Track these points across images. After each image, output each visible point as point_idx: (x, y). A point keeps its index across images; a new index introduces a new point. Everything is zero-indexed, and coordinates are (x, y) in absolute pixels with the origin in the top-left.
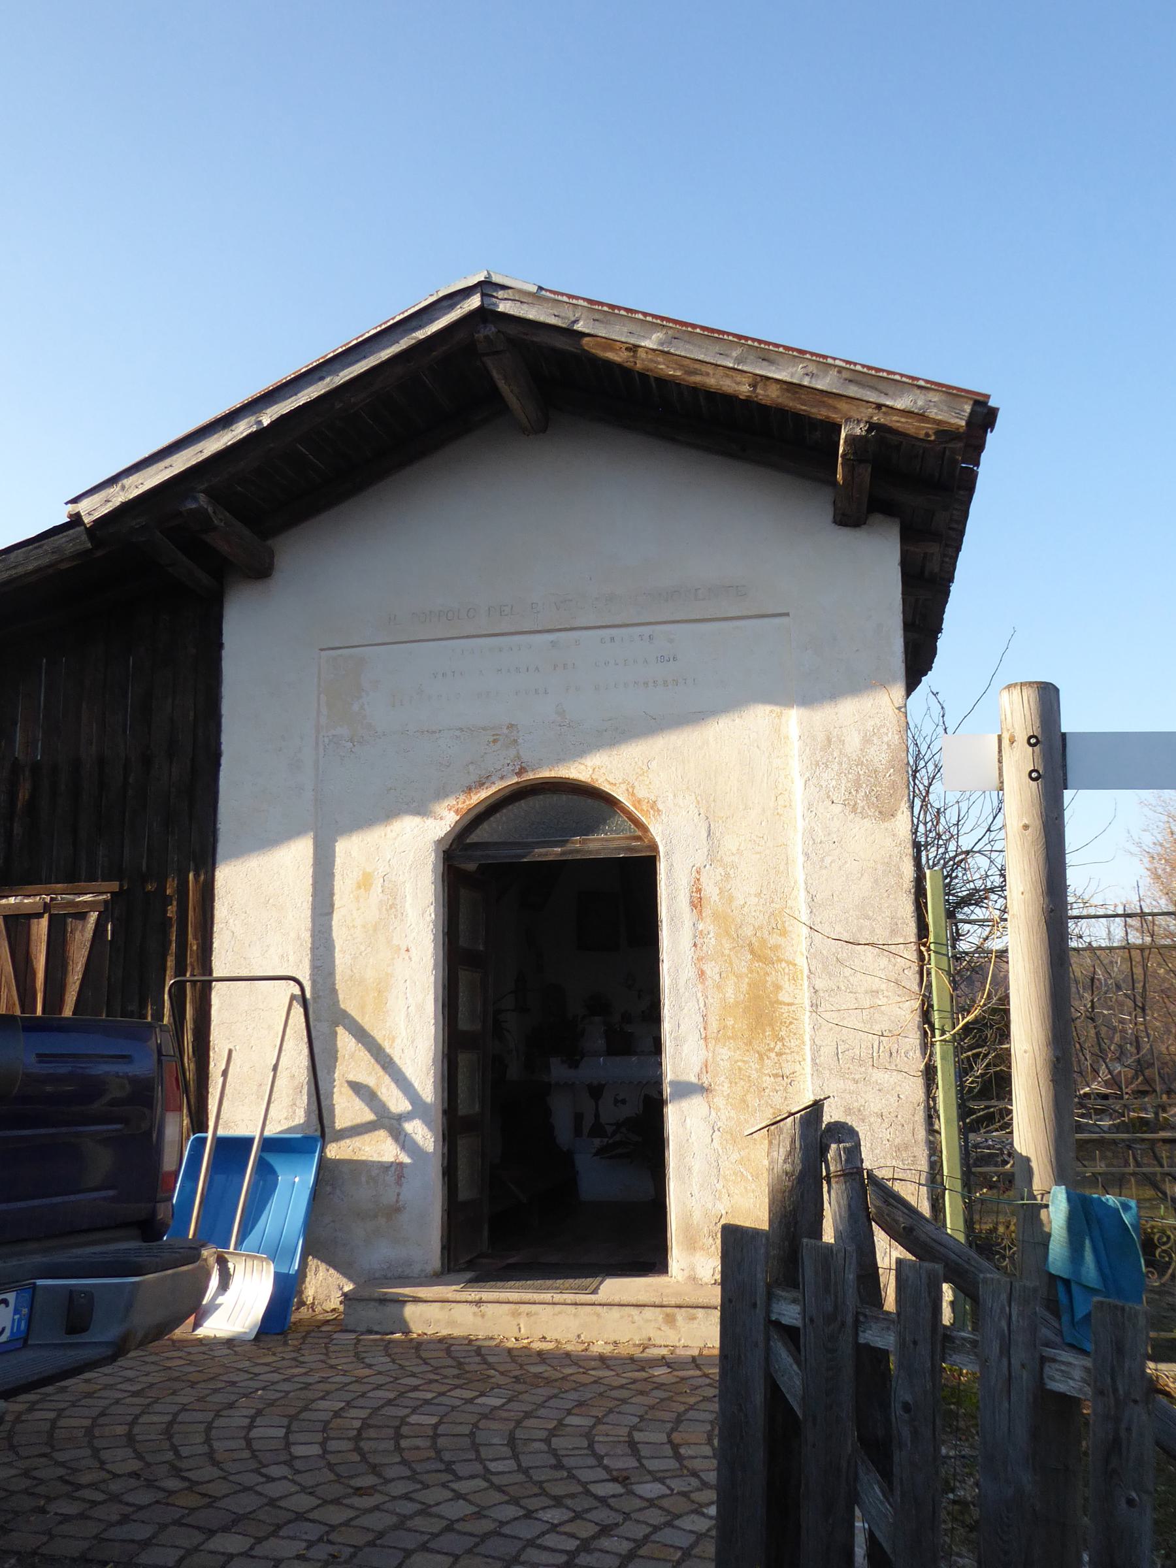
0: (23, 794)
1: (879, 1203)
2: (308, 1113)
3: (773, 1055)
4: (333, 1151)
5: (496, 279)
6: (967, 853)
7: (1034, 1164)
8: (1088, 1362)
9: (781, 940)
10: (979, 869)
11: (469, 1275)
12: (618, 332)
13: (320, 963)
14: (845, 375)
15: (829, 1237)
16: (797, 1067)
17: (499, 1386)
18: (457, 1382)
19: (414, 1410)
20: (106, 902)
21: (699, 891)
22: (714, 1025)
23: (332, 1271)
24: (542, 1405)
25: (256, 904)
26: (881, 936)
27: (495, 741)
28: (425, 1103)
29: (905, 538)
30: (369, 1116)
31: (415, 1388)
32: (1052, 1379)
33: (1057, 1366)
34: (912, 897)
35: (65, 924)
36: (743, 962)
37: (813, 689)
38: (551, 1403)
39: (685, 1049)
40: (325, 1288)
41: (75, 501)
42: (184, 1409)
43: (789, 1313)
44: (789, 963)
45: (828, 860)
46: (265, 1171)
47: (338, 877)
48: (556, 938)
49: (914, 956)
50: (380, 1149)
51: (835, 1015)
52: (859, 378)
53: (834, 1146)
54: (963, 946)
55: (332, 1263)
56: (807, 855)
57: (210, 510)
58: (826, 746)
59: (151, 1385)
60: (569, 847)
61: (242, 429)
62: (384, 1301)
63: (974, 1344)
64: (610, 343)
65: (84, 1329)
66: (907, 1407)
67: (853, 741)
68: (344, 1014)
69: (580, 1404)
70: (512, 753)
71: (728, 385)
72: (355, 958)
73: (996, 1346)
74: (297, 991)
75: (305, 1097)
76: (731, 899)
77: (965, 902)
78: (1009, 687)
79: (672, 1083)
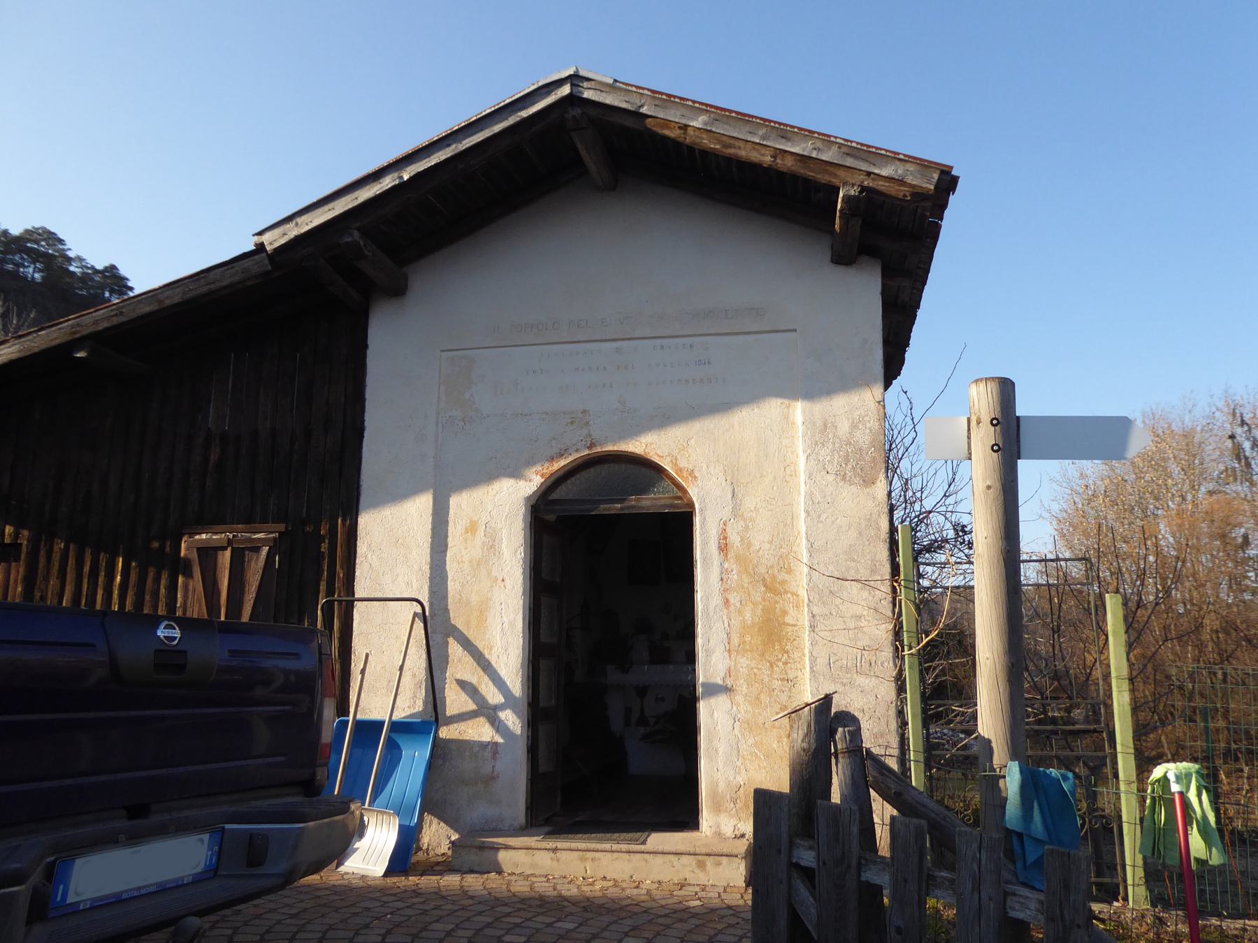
0: (214, 457)
1: (875, 774)
2: (425, 703)
3: (780, 664)
4: (444, 733)
5: (582, 73)
6: (930, 512)
7: (994, 745)
8: (1042, 897)
9: (787, 577)
10: (940, 525)
11: (547, 829)
12: (674, 115)
13: (437, 586)
14: (844, 150)
15: (836, 797)
16: (799, 673)
17: (572, 914)
18: (540, 910)
19: (508, 932)
20: (275, 539)
21: (725, 538)
22: (735, 641)
23: (442, 824)
24: (604, 929)
25: (390, 543)
26: (864, 574)
27: (572, 423)
28: (515, 697)
29: (885, 275)
30: (472, 706)
31: (508, 915)
32: (1013, 909)
33: (1016, 899)
34: (887, 545)
35: (244, 556)
36: (758, 593)
37: (812, 390)
38: (613, 927)
39: (714, 658)
40: (437, 837)
41: (260, 233)
42: (331, 928)
43: (807, 857)
44: (793, 594)
45: (824, 517)
46: (392, 746)
47: (451, 524)
48: (616, 571)
49: (889, 590)
50: (480, 731)
51: (828, 634)
52: (855, 152)
53: (840, 730)
54: (925, 583)
55: (442, 818)
56: (807, 512)
57: (362, 243)
58: (821, 432)
59: (305, 910)
60: (627, 504)
61: (388, 182)
62: (482, 847)
63: (952, 881)
64: (666, 123)
65: (260, 864)
66: (899, 931)
67: (844, 427)
68: (455, 628)
69: (634, 928)
70: (585, 431)
71: (755, 156)
72: (463, 586)
73: (969, 885)
74: (419, 610)
75: (423, 691)
76: (749, 545)
77: (929, 549)
78: (976, 381)
79: (704, 685)
